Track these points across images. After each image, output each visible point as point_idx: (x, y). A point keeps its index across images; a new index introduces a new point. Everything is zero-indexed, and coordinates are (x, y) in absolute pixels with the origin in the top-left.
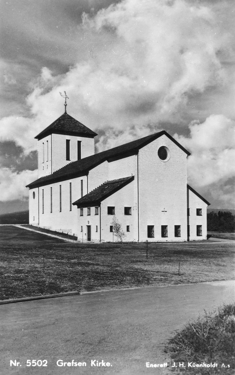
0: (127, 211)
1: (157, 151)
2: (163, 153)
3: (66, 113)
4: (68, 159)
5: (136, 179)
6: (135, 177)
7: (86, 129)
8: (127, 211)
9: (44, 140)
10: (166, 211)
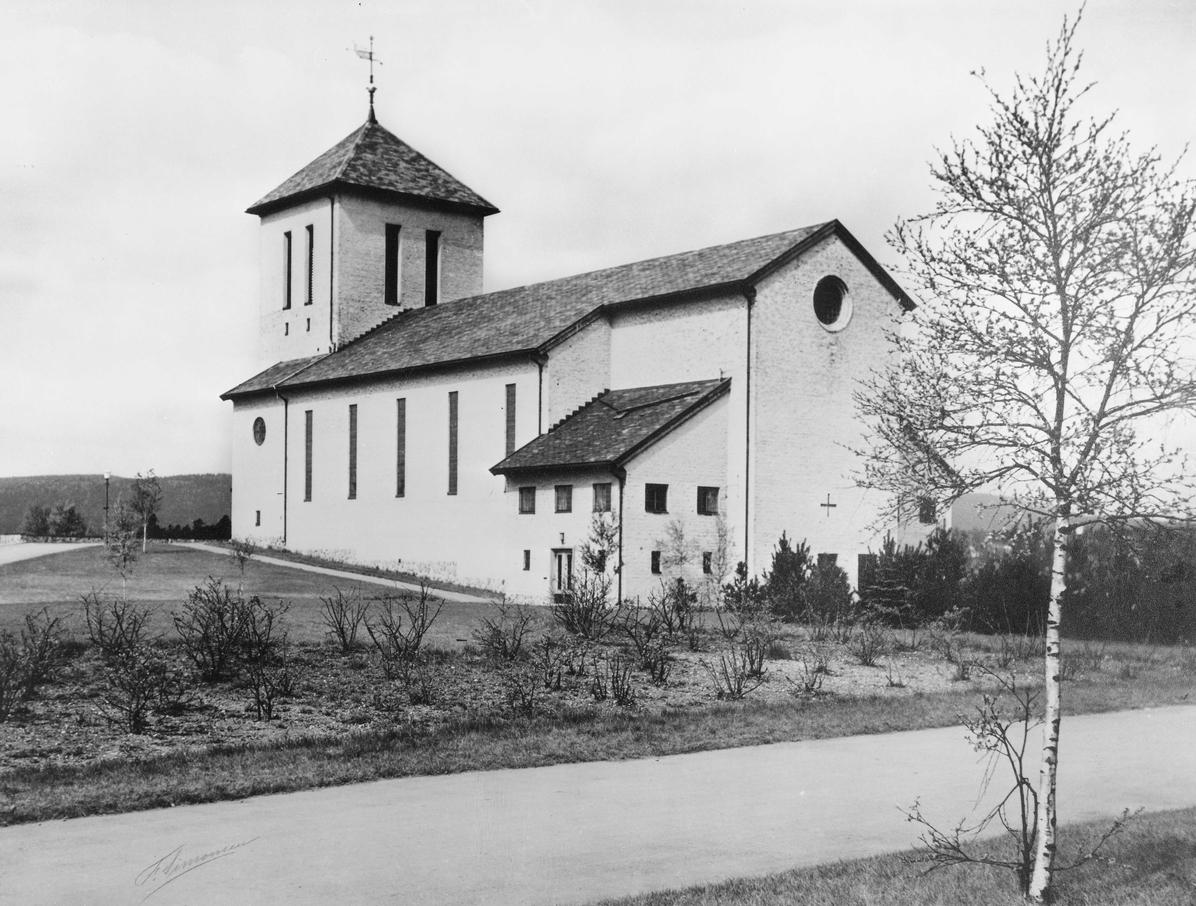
0: (707, 499)
1: (813, 293)
2: (829, 298)
3: (372, 119)
4: (391, 298)
5: (738, 389)
6: (733, 381)
7: (453, 186)
8: (707, 499)
9: (295, 221)
10: (835, 506)
